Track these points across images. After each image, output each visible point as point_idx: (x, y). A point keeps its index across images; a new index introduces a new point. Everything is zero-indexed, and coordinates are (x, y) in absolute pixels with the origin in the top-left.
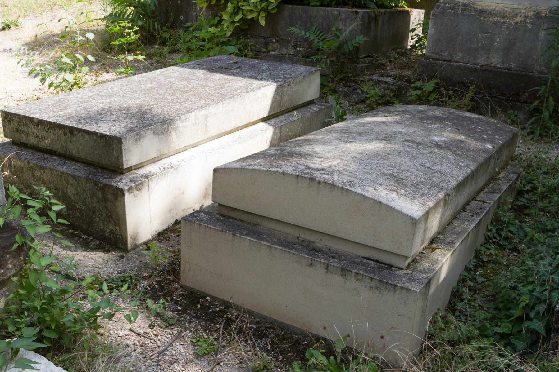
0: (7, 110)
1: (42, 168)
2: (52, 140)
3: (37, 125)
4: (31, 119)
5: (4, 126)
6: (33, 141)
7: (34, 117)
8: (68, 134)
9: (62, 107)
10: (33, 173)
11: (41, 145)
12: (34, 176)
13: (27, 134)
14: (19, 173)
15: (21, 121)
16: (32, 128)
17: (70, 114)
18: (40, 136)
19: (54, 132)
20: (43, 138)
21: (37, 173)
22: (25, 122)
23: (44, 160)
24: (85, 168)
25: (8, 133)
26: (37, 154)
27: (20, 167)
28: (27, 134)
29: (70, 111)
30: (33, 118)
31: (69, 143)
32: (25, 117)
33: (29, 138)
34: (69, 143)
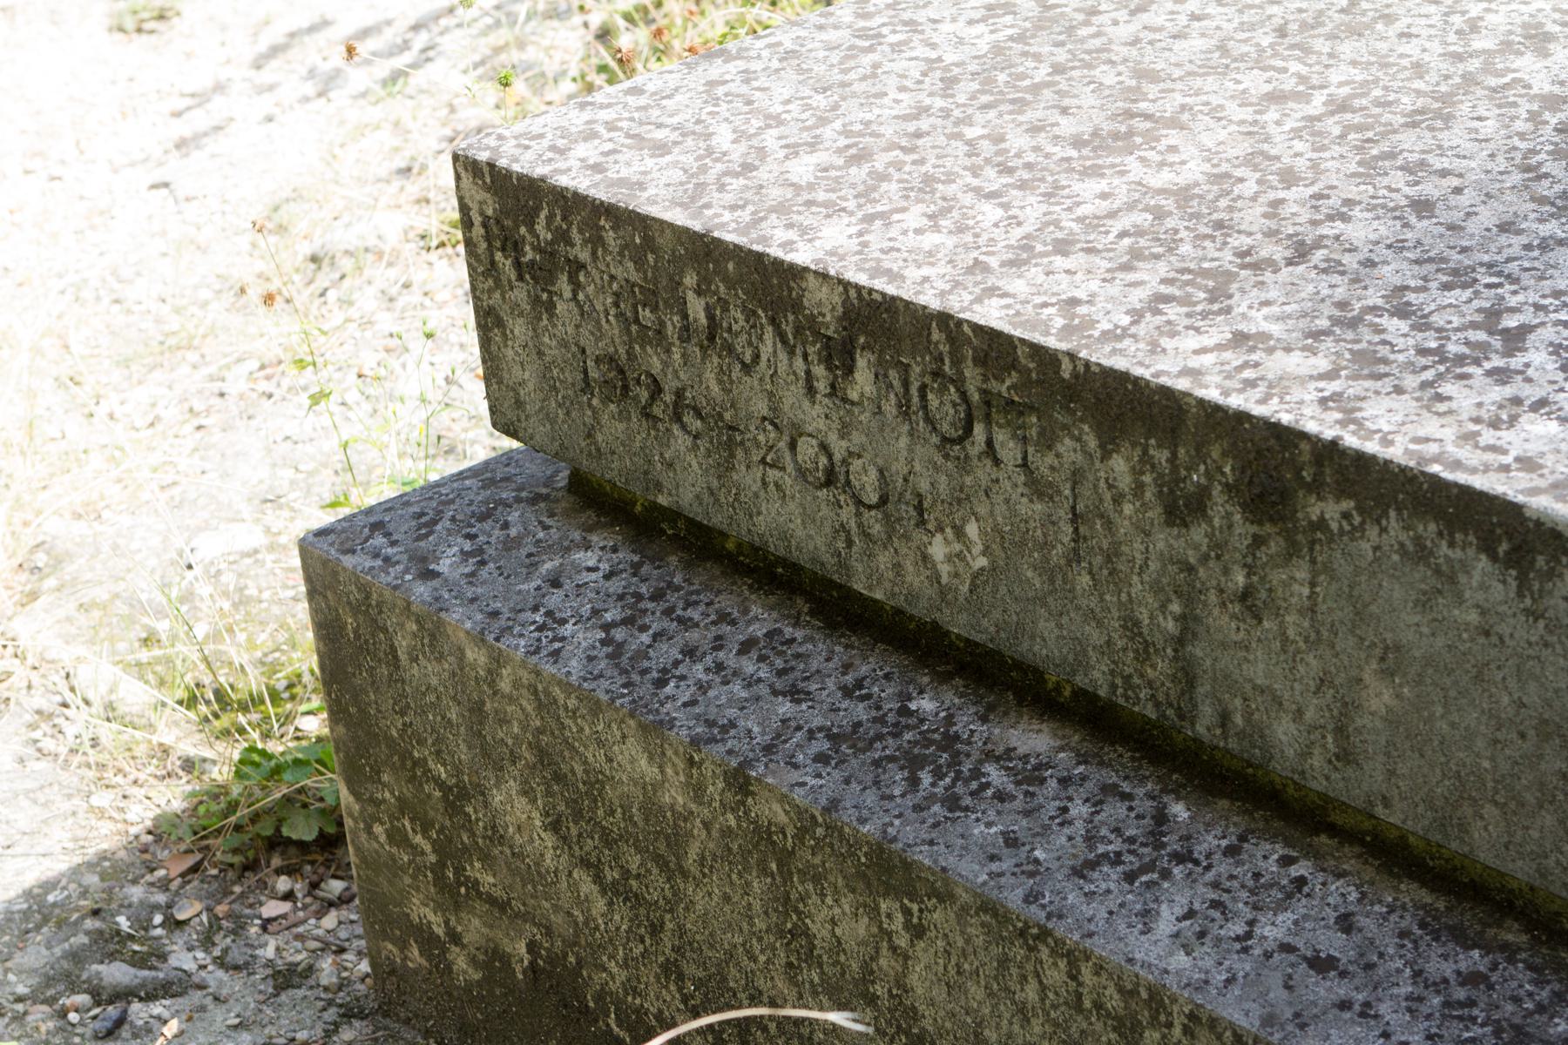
0: (524, 162)
1: (886, 872)
2: (1009, 542)
3: (840, 357)
4: (770, 285)
5: (489, 322)
6: (789, 518)
7: (802, 256)
8: (1220, 505)
9: (1090, 111)
10: (786, 904)
11: (876, 576)
12: (801, 931)
13: (726, 437)
14: (634, 862)
15: (657, 293)
16: (779, 383)
17: (1205, 209)
18: (867, 483)
19: (1043, 463)
20: (903, 509)
21: (838, 919)
22: (697, 308)
23: (913, 764)
24: (1439, 965)
25: (530, 392)
26: (822, 655)
27: (651, 809)
28: (726, 437)
29: (1194, 170)
30: (795, 273)
31: (1222, 622)
32: (704, 251)
33: (748, 478)
34: (1222, 622)
